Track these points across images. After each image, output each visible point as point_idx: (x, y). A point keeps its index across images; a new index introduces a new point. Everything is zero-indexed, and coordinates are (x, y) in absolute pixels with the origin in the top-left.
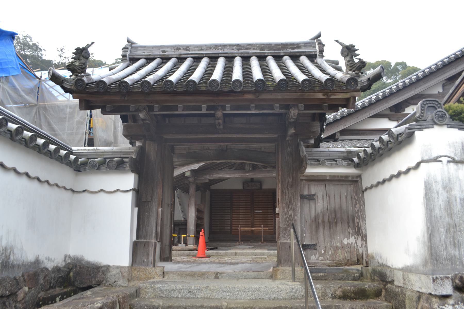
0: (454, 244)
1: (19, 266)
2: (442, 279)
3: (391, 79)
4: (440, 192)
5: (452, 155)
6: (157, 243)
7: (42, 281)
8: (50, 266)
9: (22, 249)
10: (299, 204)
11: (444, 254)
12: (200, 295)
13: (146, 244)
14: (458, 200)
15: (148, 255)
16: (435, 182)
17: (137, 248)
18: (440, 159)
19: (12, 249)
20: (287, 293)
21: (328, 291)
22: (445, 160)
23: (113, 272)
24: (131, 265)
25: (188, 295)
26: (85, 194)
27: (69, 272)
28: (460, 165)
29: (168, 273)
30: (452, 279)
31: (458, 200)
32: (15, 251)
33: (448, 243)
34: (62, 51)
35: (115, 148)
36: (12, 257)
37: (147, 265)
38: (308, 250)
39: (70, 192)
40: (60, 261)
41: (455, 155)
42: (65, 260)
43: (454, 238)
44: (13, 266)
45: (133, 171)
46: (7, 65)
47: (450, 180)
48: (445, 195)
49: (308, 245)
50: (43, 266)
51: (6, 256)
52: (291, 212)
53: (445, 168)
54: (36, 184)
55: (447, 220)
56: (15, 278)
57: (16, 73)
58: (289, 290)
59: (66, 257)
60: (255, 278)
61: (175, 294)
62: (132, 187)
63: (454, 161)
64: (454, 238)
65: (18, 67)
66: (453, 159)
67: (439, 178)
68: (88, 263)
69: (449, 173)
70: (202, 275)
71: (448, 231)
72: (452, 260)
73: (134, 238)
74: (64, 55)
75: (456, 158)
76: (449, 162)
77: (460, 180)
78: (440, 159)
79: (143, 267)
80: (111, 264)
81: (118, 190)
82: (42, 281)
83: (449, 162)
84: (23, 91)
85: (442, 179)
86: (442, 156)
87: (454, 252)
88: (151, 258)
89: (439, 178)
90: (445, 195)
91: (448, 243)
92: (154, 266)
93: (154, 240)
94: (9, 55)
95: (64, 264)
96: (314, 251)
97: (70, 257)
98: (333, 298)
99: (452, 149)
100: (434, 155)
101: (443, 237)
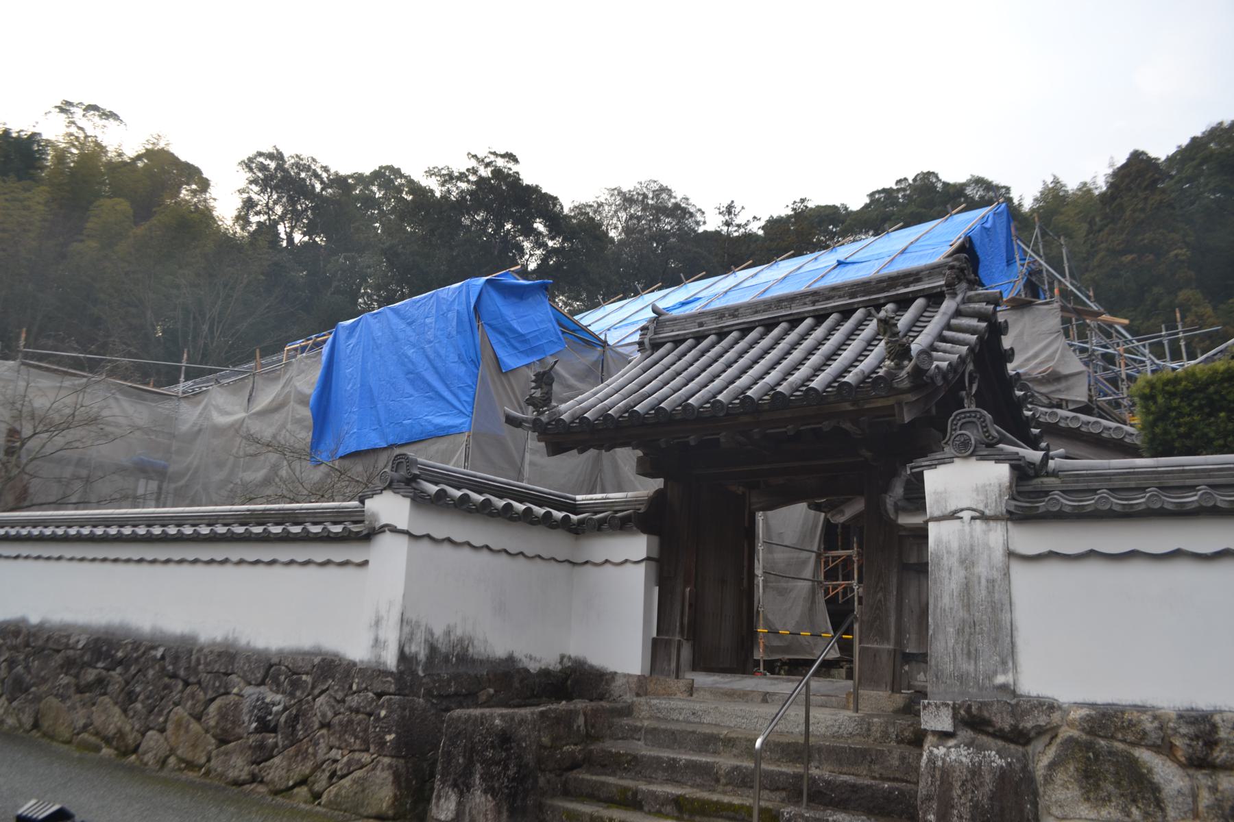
0: (969, 652)
1: (481, 662)
2: (937, 707)
3: (937, 367)
4: (954, 569)
5: (981, 507)
6: (685, 642)
7: (517, 685)
8: (533, 667)
9: (486, 641)
10: (894, 580)
11: (949, 668)
12: (707, 720)
13: (668, 643)
14: (983, 582)
15: (670, 660)
16: (949, 552)
17: (658, 649)
18: (960, 515)
19: (471, 640)
20: (827, 727)
21: (891, 730)
22: (966, 515)
23: (619, 681)
24: (647, 673)
25: (692, 718)
26: (588, 567)
27: (567, 679)
28: (992, 524)
29: (697, 689)
30: (954, 708)
31: (983, 582)
32: (476, 643)
33: (958, 651)
34: (730, 213)
35: (630, 494)
36: (471, 650)
37: (668, 675)
38: (914, 664)
39: (567, 565)
40: (553, 663)
41: (986, 506)
42: (561, 662)
43: (969, 643)
44: (473, 661)
45: (644, 532)
46: (539, 340)
47: (972, 550)
48: (962, 573)
49: (913, 654)
50: (521, 666)
51: (462, 648)
52: (880, 595)
53: (967, 528)
54: (504, 558)
55: (962, 614)
56: (476, 676)
57: (558, 349)
58: (829, 723)
59: (562, 657)
60: (821, 706)
61: (675, 716)
62: (644, 556)
63: (983, 517)
64: (969, 643)
65: (559, 339)
66: (983, 513)
67: (955, 546)
68: (592, 667)
69: (972, 537)
70: (744, 696)
71: (960, 632)
72: (962, 678)
73: (654, 634)
74: (737, 221)
75: (987, 512)
76: (973, 518)
77: (989, 548)
78: (960, 515)
79: (662, 678)
80: (619, 671)
81: (626, 561)
82: (517, 685)
83: (973, 518)
84: (574, 376)
85: (960, 547)
86: (962, 510)
87: (967, 667)
88: (673, 665)
89: (955, 546)
90: (962, 573)
91: (958, 651)
92: (677, 677)
93: (677, 638)
94: (542, 322)
95: (559, 667)
96: (923, 665)
97: (570, 658)
98: (899, 742)
99: (982, 497)
100: (952, 507)
101: (951, 642)
